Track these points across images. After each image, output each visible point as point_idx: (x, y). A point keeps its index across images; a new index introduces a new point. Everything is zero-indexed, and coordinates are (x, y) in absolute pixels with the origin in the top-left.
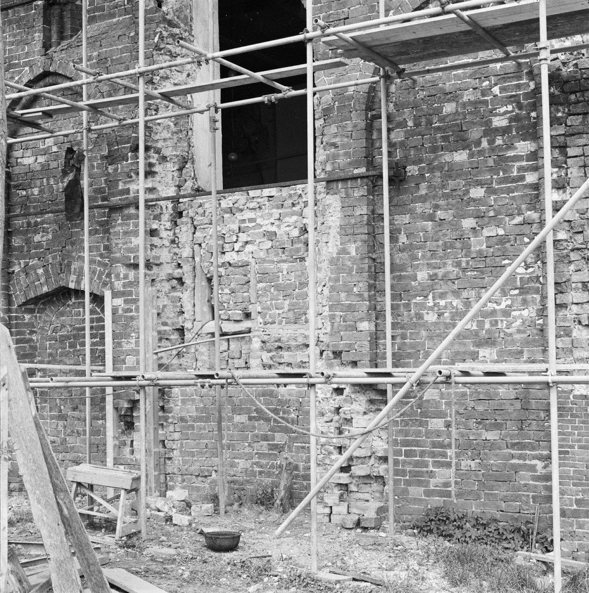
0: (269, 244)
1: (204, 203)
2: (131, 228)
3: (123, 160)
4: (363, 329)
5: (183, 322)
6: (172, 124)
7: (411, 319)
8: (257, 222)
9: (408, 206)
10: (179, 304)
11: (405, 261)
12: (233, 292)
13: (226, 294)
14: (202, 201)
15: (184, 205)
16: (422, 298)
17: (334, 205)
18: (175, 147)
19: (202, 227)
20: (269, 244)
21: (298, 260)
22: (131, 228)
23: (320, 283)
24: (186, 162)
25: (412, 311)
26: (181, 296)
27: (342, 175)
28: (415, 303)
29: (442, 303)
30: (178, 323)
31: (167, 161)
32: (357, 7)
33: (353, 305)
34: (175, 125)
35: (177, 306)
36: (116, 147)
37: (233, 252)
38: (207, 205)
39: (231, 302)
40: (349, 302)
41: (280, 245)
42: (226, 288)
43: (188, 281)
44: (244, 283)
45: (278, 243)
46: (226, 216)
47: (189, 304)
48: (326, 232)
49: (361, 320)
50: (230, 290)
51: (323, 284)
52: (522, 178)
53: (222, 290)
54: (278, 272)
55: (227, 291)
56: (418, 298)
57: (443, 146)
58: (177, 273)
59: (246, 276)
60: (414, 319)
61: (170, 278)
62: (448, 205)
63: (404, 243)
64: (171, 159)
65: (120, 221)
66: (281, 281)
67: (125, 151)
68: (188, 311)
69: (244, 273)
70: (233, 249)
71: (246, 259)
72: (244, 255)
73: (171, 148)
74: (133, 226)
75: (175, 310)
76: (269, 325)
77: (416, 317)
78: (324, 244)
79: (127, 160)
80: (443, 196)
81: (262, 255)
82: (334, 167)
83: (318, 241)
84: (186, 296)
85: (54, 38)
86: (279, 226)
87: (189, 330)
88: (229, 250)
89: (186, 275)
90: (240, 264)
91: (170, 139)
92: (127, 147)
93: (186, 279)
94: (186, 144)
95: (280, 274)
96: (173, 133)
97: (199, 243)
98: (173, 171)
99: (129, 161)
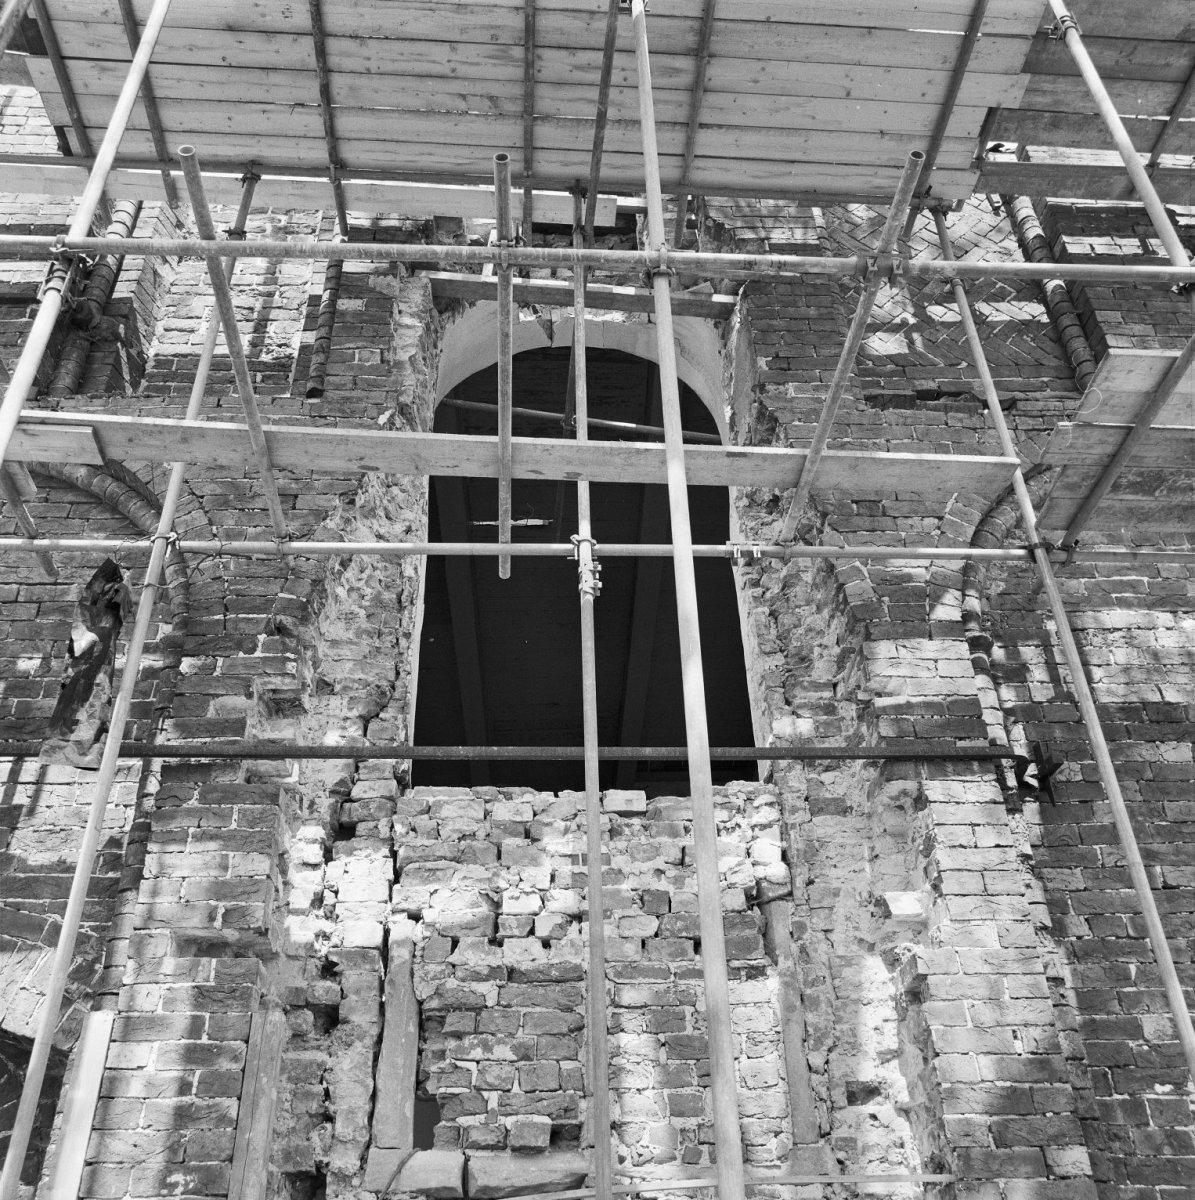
0: (652, 925)
1: (439, 805)
2: (234, 826)
3: (239, 646)
4: (1073, 1171)
5: (327, 1151)
6: (362, 613)
7: (1158, 1150)
8: (613, 866)
9: (1074, 848)
10: (319, 1089)
11: (1098, 985)
12: (526, 1058)
13: (499, 1062)
14: (431, 800)
15: (363, 807)
16: (1168, 1088)
17: (839, 840)
18: (362, 662)
19: (429, 865)
20: (652, 925)
21: (743, 973)
22: (234, 826)
23: (819, 1042)
24: (383, 707)
25: (1152, 1127)
26: (330, 1062)
27: (921, 748)
28: (1156, 1101)
30: (307, 1152)
31: (332, 693)
32: (906, 441)
33: (1023, 1091)
34: (368, 616)
35: (308, 1095)
36: (221, 617)
37: (531, 938)
38: (445, 812)
39: (516, 1089)
40: (1008, 1084)
41: (687, 929)
42: (500, 1042)
43: (360, 1016)
44: (565, 1030)
45: (679, 924)
46: (510, 843)
47: (359, 1090)
48: (825, 903)
49: (1060, 1140)
50: (515, 1049)
51: (829, 1042)
53: (487, 1048)
54: (682, 1003)
55: (503, 1052)
56: (1158, 1088)
57: (1131, 729)
58: (324, 990)
59: (570, 1010)
60: (1167, 1150)
61: (295, 1004)
62: (1178, 852)
63: (1079, 938)
64: (345, 688)
65: (193, 803)
66: (689, 1031)
67: (248, 629)
68: (351, 1112)
69: (564, 1001)
70: (532, 932)
71: (577, 961)
72: (567, 950)
73: (350, 665)
74: (238, 822)
75: (301, 1107)
76: (648, 1167)
77: (1171, 1145)
78: (821, 935)
79: (253, 650)
80: (1159, 834)
81: (631, 950)
82: (901, 730)
83: (800, 928)
84: (347, 1066)
85: (65, 380)
86: (678, 881)
87: (343, 1178)
88: (516, 932)
89: (353, 997)
90: (554, 973)
91: (351, 642)
92: (258, 621)
93: (352, 1009)
94: (390, 664)
95: (688, 1010)
96: (359, 633)
97: (413, 907)
98: (346, 719)
99: (258, 654)
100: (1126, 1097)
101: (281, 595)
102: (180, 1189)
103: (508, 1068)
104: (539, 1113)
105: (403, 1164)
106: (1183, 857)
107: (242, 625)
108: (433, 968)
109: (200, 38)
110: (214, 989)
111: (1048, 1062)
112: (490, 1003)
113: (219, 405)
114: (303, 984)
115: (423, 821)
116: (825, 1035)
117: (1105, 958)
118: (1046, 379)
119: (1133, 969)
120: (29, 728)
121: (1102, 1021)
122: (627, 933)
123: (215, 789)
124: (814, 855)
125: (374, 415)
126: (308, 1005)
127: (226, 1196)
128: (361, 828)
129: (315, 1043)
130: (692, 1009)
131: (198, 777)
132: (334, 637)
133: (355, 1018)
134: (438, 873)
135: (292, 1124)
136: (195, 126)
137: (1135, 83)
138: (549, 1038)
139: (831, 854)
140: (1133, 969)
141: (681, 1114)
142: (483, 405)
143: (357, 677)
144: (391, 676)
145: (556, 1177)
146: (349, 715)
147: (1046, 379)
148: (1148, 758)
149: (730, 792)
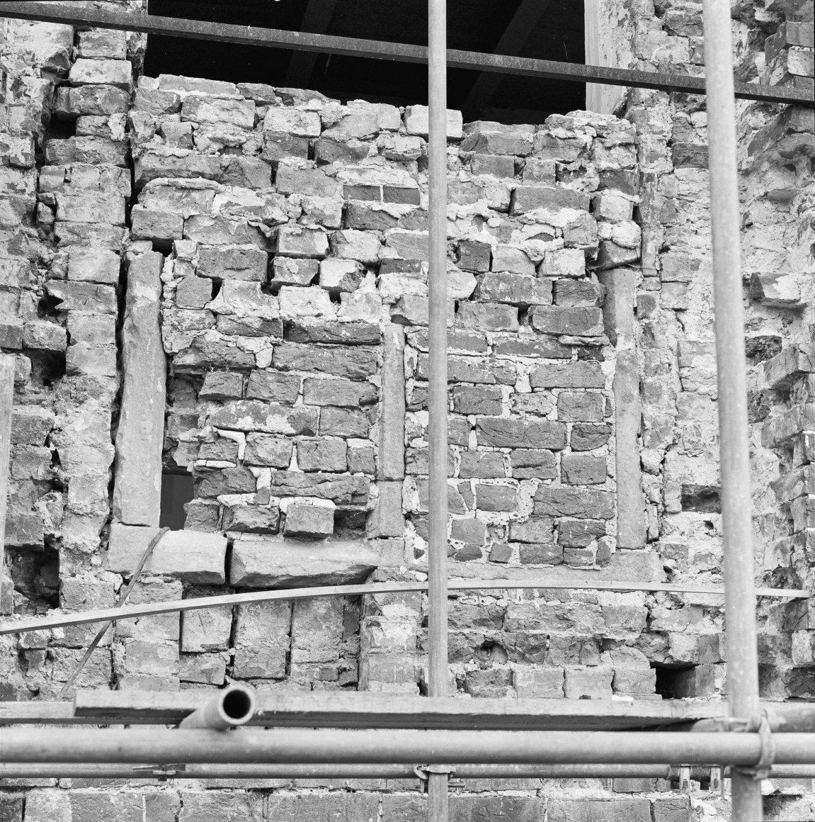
0: (468, 284)
1: (195, 103)
5: (58, 524)
10: (46, 452)
14: (183, 95)
20: (468, 284)
41: (511, 293)
42: (274, 411)
44: (355, 403)
48: (679, 277)
51: (669, 440)
53: (259, 417)
66: (506, 414)
71: (374, 320)
83: (648, 303)
86: (503, 234)
90: (345, 334)
104: (321, 496)
108: (189, 316)
112: (262, 363)
115: (172, 123)
130: (511, 390)
133: (87, 369)
139: (692, 217)
141: (489, 508)
145: (340, 568)
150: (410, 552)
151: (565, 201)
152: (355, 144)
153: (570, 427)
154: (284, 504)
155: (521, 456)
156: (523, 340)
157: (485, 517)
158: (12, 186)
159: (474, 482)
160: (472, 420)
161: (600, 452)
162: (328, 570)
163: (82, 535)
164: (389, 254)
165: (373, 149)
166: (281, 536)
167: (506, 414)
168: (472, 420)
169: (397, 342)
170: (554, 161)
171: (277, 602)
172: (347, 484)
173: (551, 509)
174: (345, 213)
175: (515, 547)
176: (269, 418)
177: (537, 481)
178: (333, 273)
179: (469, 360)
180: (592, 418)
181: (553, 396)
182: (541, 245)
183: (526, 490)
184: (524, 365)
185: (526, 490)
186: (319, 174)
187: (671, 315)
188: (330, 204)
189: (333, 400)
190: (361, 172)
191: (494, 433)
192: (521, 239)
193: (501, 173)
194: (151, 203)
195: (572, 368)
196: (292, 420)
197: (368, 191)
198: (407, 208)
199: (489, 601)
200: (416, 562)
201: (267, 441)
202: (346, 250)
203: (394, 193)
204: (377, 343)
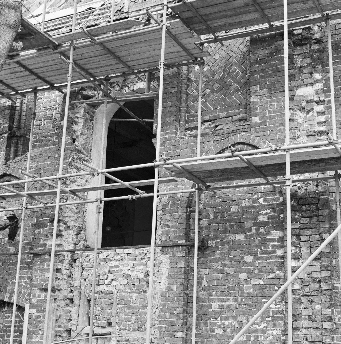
0: (126, 281)
1: (90, 255)
2: (45, 267)
3: (44, 226)
4: (178, 337)
5: (71, 326)
6: (75, 208)
7: (207, 332)
10: (69, 315)
11: (205, 297)
12: (102, 309)
14: (88, 254)
17: (165, 261)
18: (75, 221)
20: (126, 281)
21: (142, 292)
22: (45, 267)
23: (155, 307)
24: (81, 231)
27: (171, 243)
29: (226, 323)
32: (185, 149)
34: (76, 209)
35: (68, 316)
36: (41, 219)
39: (101, 315)
41: (132, 282)
42: (98, 306)
43: (76, 301)
44: (109, 304)
45: (131, 281)
48: (160, 276)
49: (178, 331)
50: (101, 308)
51: (156, 307)
52: (275, 252)
53: (96, 308)
55: (99, 308)
56: (212, 319)
60: (209, 332)
64: (72, 228)
65: (39, 263)
66: (131, 304)
67: (46, 222)
70: (105, 283)
71: (112, 290)
75: (67, 318)
79: (47, 227)
80: (229, 260)
81: (121, 288)
82: (167, 239)
83: (155, 281)
84: (74, 310)
85: (12, 155)
86: (132, 271)
87: (74, 331)
88: (102, 283)
89: (75, 297)
90: (108, 292)
94: (82, 220)
98: (73, 235)
99: (48, 228)
100: (205, 321)
101: (52, 213)
102: (40, 334)
103: (99, 311)
104: (104, 320)
105: (82, 329)
106: (232, 266)
107: (45, 221)
108: (88, 291)
109: (8, 75)
110: (44, 299)
111: (179, 315)
112: (97, 298)
113: (38, 161)
114: (66, 295)
115: (87, 259)
116: (156, 306)
117: (208, 290)
118: (241, 110)
119: (214, 293)
120: (16, 244)
121: (204, 305)
122: (121, 284)
123: (42, 259)
124: (160, 264)
125: (68, 159)
126: (68, 299)
127: (9, 343)
128: (77, 260)
129: (70, 306)
130: (132, 300)
131: (39, 257)
132: (69, 215)
133: (75, 301)
134: (89, 271)
135: (65, 321)
136: (19, 86)
137: (247, 14)
138: (107, 306)
139: (163, 264)
140: (214, 293)
141: (128, 321)
142: (121, 119)
143: (74, 225)
144: (82, 223)
145: (107, 332)
146: (73, 234)
147: (241, 110)
148: (232, 239)
149: (145, 249)
150: (116, 329)
151: (141, 265)
152: (111, 259)
153: (141, 306)
154: (99, 321)
155: (133, 312)
156: (134, 291)
157: (128, 323)
158: (67, 273)
159: (126, 317)
160: (126, 306)
161: (146, 310)
162: (105, 332)
163: (74, 328)
164: (114, 278)
165: (114, 259)
166: (101, 327)
167: (131, 304)
168: (126, 306)
169: (116, 292)
170: (141, 257)
171: (103, 337)
172: (108, 318)
173: (137, 321)
174: (109, 271)
175: (131, 328)
176: (98, 308)
177: (135, 316)
178: (107, 282)
179: (126, 295)
180: (144, 304)
181: (139, 300)
182: (137, 273)
183: (134, 317)
184: (134, 295)
185: (134, 317)
186: (106, 265)
187: (158, 283)
188: (107, 270)
189: (106, 304)
190: (112, 263)
191: (129, 308)
192: (135, 273)
193: (132, 260)
194: (84, 273)
195: (142, 295)
196: (101, 308)
197: (112, 267)
198: (118, 269)
199: (126, 337)
200: (117, 331)
201: (97, 311)
202: (109, 278)
203: (116, 267)
204: (112, 293)
